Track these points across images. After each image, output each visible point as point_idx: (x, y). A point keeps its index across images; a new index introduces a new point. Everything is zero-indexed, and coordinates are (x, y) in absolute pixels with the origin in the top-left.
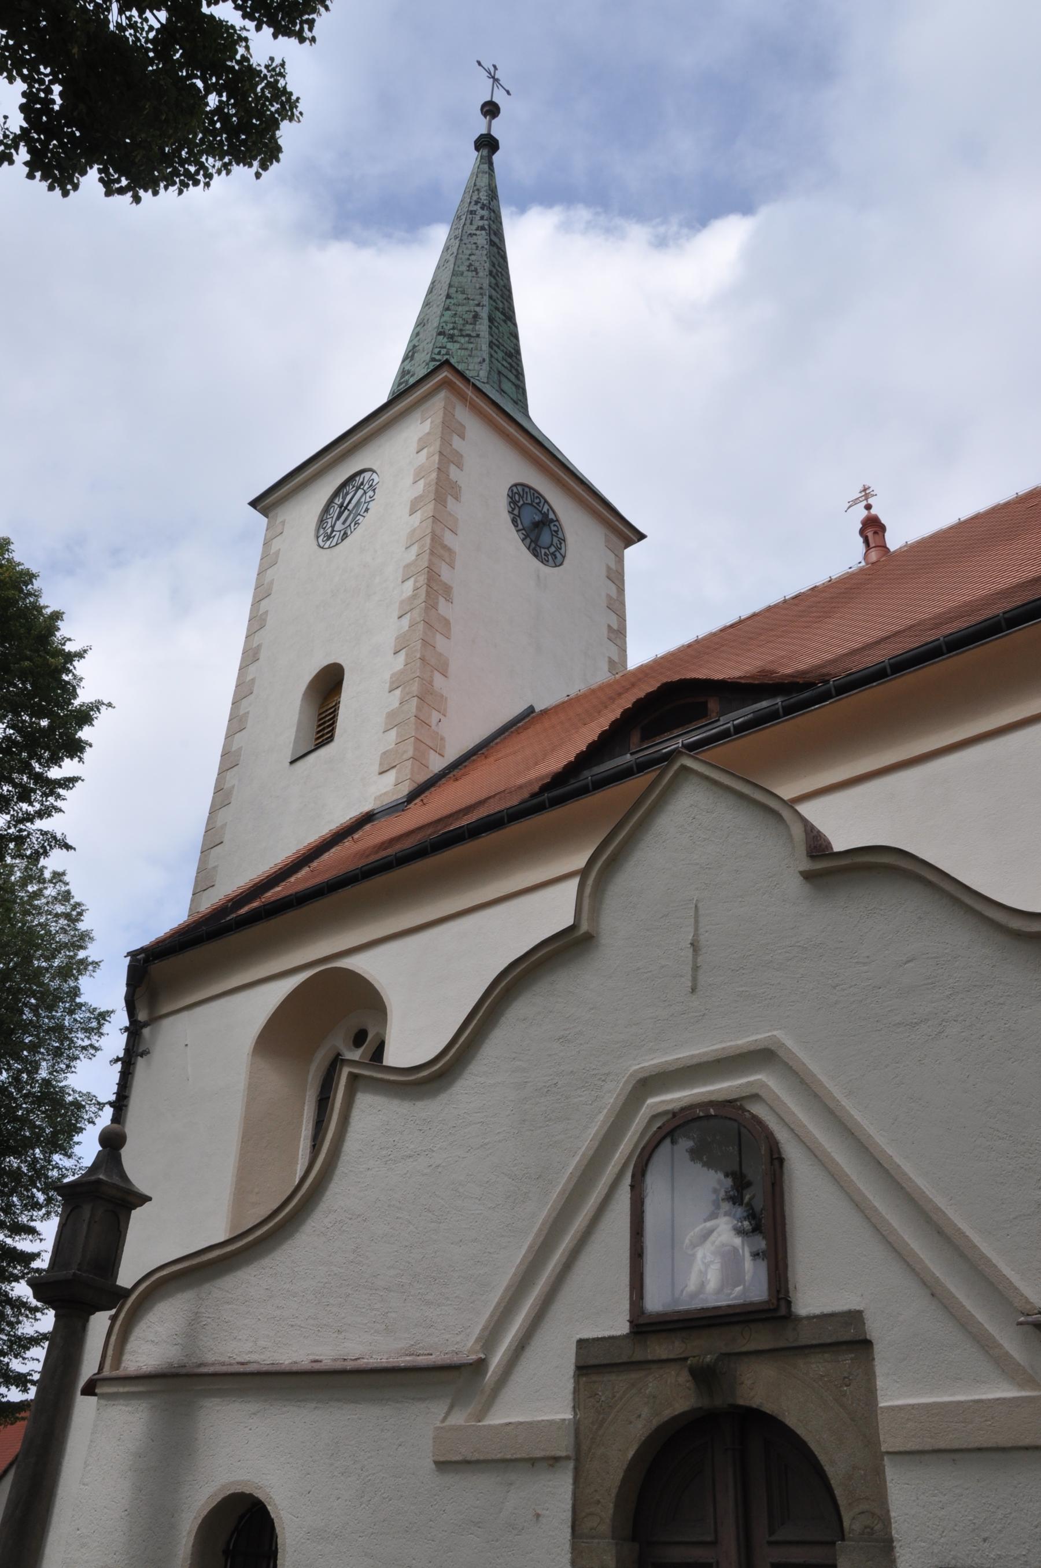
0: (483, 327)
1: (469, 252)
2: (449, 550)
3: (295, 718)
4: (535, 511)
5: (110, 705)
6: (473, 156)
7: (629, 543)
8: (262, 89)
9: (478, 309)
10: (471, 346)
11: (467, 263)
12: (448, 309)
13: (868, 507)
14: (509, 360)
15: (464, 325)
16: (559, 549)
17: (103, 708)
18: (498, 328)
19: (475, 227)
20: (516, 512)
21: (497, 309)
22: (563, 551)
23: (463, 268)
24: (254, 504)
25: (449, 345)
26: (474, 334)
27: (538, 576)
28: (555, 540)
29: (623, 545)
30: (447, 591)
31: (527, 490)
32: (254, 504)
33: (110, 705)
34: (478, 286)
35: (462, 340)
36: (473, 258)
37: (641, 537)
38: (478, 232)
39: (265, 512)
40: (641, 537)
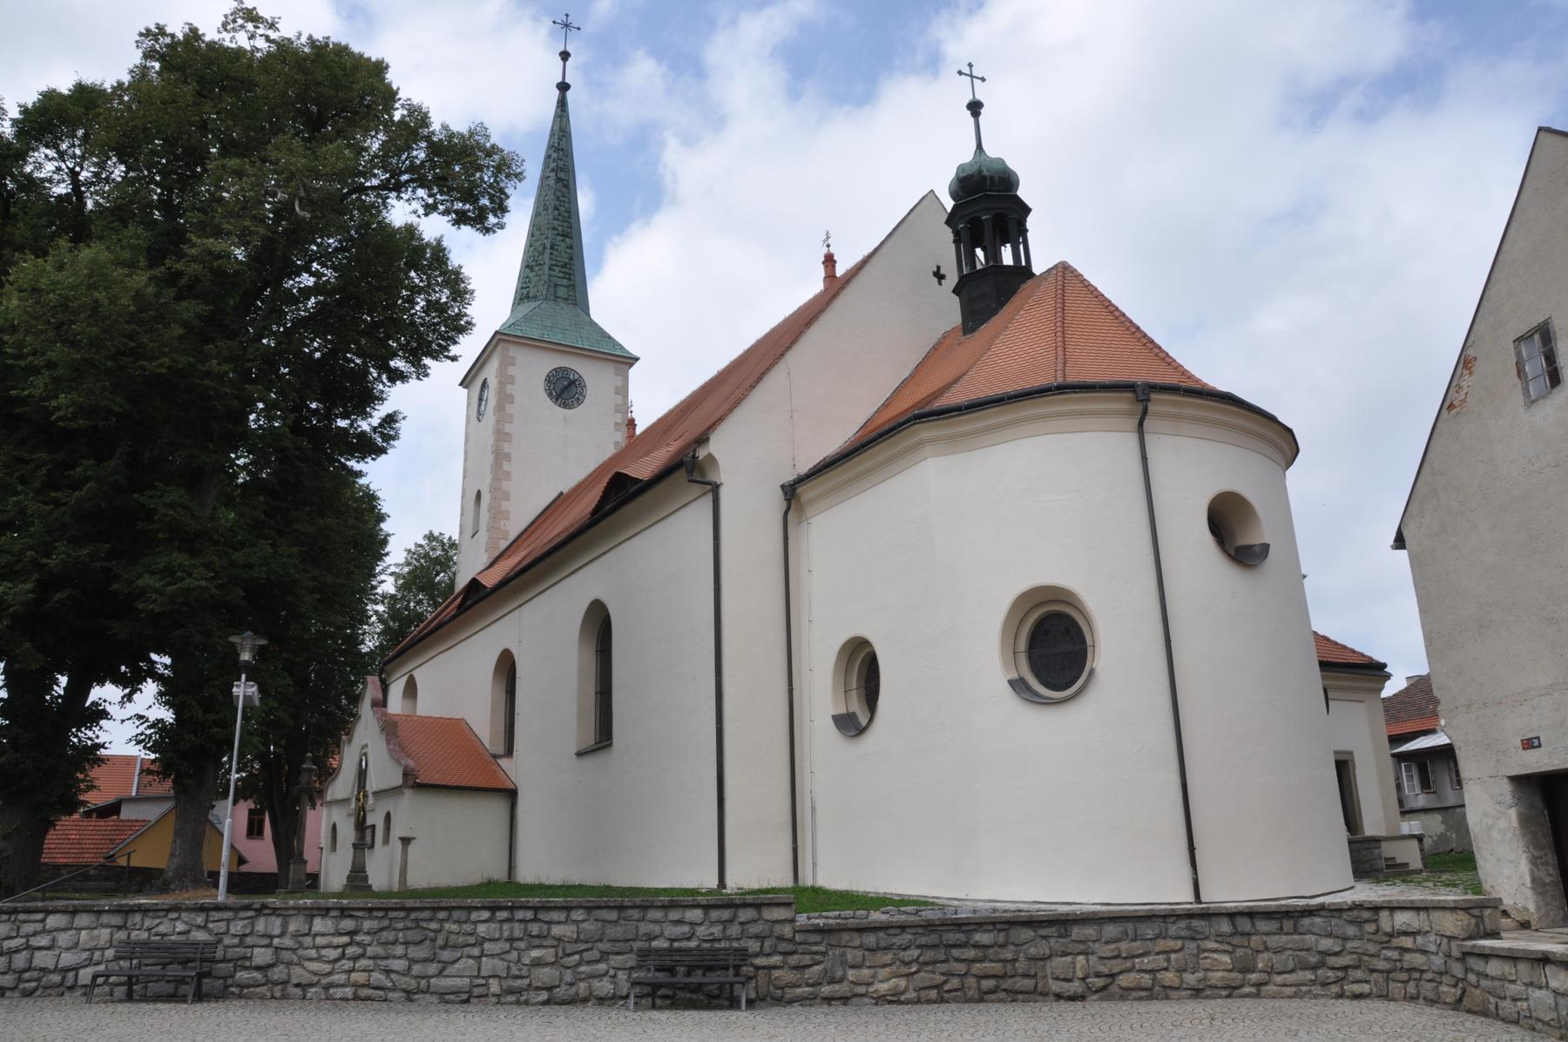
0: (547, 256)
2: (507, 434)
25: (531, 275)
30: (508, 457)
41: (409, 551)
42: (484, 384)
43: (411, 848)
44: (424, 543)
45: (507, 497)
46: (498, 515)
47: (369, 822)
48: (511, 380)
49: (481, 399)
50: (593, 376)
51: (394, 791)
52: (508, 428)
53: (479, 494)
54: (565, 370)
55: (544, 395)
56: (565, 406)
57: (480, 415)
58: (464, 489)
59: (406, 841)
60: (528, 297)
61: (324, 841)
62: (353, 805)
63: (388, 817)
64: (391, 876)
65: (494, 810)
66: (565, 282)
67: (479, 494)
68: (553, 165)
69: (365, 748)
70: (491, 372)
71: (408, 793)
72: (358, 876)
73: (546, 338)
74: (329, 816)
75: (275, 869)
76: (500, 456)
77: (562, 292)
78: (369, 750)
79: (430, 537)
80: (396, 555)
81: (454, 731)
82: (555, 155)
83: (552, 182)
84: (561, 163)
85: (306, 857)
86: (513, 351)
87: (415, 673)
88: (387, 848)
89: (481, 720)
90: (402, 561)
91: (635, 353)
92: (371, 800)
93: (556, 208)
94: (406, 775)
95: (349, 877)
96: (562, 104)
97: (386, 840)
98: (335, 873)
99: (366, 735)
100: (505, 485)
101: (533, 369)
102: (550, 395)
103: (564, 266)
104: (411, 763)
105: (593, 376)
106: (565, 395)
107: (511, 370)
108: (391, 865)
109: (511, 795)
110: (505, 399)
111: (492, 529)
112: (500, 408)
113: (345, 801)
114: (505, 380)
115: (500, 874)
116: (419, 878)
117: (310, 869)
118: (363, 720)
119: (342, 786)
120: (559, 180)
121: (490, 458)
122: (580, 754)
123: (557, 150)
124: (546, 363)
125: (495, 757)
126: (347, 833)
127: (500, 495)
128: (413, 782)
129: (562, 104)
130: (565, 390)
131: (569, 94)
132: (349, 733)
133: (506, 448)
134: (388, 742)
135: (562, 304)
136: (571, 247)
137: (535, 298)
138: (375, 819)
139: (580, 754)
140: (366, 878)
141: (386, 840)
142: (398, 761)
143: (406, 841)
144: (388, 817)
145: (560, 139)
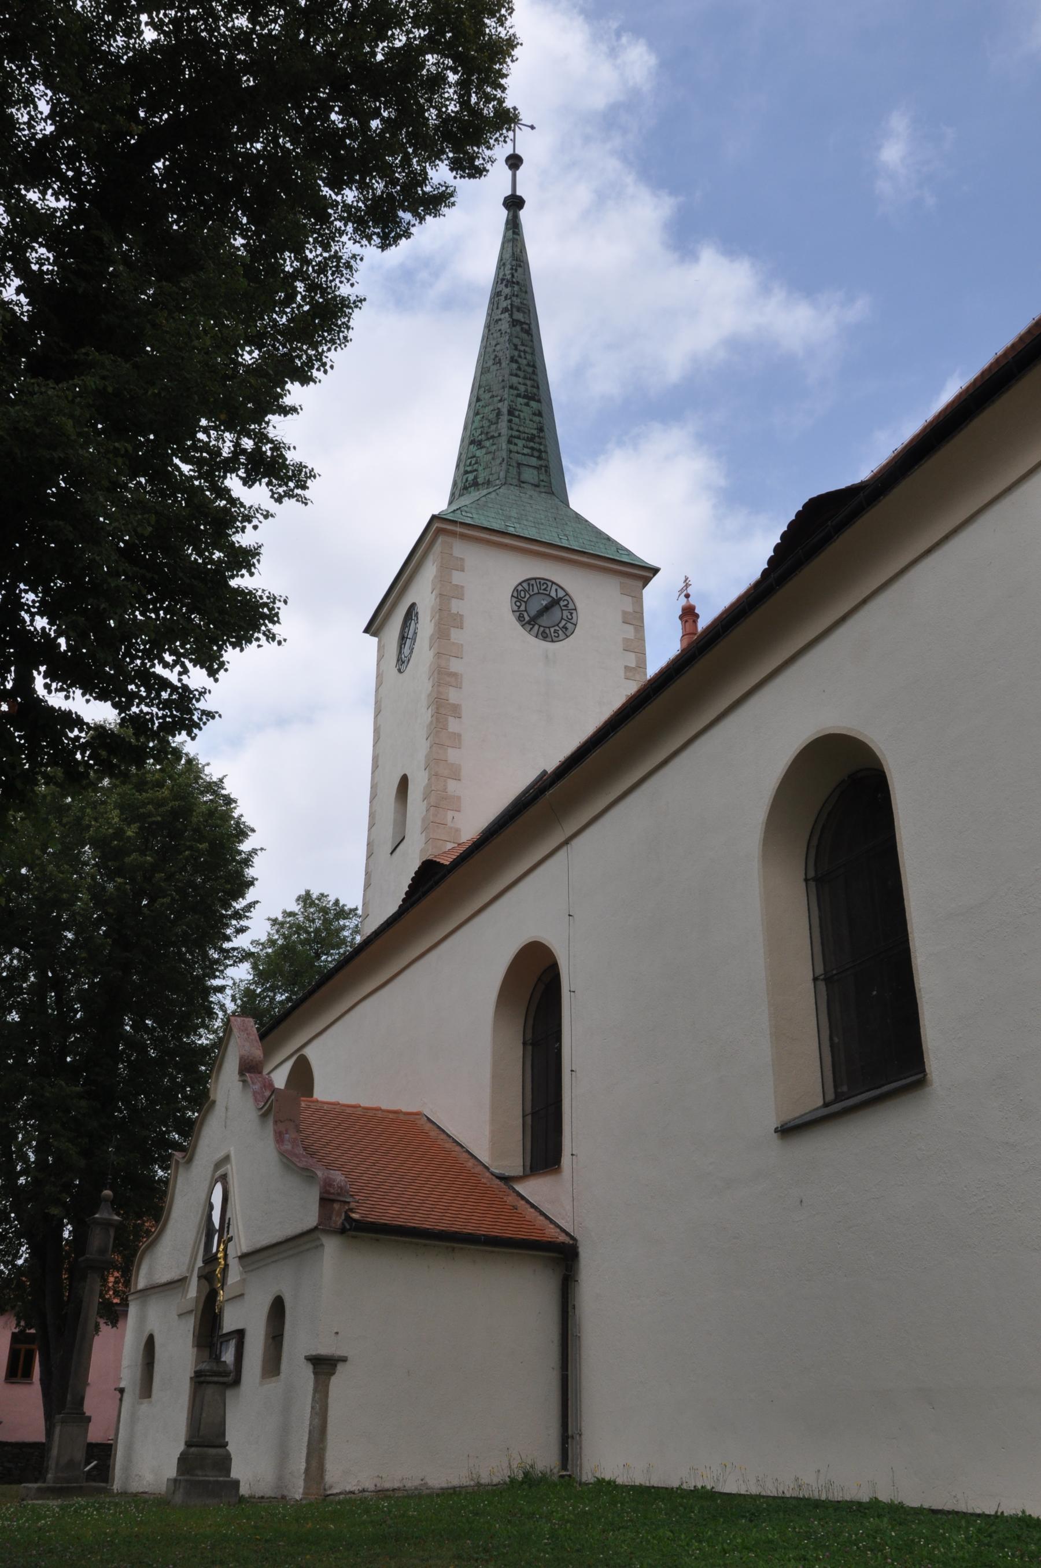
0: (503, 425)
1: (494, 343)
2: (455, 675)
3: (392, 810)
4: (543, 596)
5: (262, 849)
6: (503, 214)
7: (646, 581)
8: (171, 895)
9: (500, 405)
10: (495, 447)
11: (493, 357)
12: (477, 414)
13: (687, 596)
14: (532, 444)
15: (489, 427)
16: (569, 620)
17: (259, 852)
18: (519, 417)
19: (499, 311)
20: (523, 608)
21: (518, 396)
22: (574, 621)
23: (490, 362)
24: (366, 631)
25: (478, 453)
26: (496, 435)
27: (547, 657)
28: (565, 613)
29: (640, 584)
30: (456, 711)
31: (533, 582)
32: (366, 631)
33: (262, 849)
34: (501, 379)
35: (487, 444)
36: (498, 348)
37: (655, 571)
38: (502, 316)
39: (374, 634)
40: (655, 571)
41: (274, 922)
42: (411, 613)
43: (337, 1383)
44: (295, 908)
45: (456, 775)
46: (441, 802)
47: (230, 1323)
48: (459, 593)
49: (403, 638)
50: (590, 596)
51: (295, 1246)
52: (455, 666)
53: (404, 782)
54: (540, 584)
55: (511, 619)
56: (544, 636)
57: (402, 662)
58: (374, 787)
59: (324, 1366)
60: (475, 484)
61: (129, 1375)
62: (192, 1292)
63: (278, 1309)
64: (283, 1456)
65: (509, 1302)
66: (534, 461)
67: (404, 782)
68: (505, 304)
69: (230, 1175)
70: (423, 593)
71: (331, 1248)
72: (205, 1449)
73: (511, 530)
74: (142, 1319)
75: (42, 1438)
76: (442, 711)
77: (529, 475)
78: (233, 1169)
79: (306, 899)
80: (256, 929)
81: (409, 1136)
82: (507, 291)
83: (505, 326)
84: (517, 301)
85: (88, 1408)
86: (461, 549)
87: (309, 1052)
88: (274, 1387)
89: (469, 1105)
90: (264, 938)
91: (651, 560)
92: (234, 1275)
93: (513, 360)
94: (326, 1201)
95: (183, 1459)
96: (514, 226)
97: (273, 1365)
98: (150, 1454)
99: (232, 1130)
100: (455, 606)
101: (491, 580)
102: (520, 618)
103: (532, 438)
104: (338, 1177)
105: (590, 596)
106: (544, 621)
107: (457, 578)
108: (285, 1431)
109: (562, 1257)
110: (448, 622)
111: (429, 825)
112: (442, 634)
113: (180, 1283)
114: (448, 593)
115: (545, 1458)
116: (350, 1471)
117: (95, 1434)
118: (219, 1111)
119: (171, 1255)
120: (514, 323)
121: (426, 716)
122: (787, 1131)
123: (510, 283)
124: (514, 570)
125: (505, 1179)
126: (178, 1355)
127: (441, 769)
128: (351, 1224)
129: (514, 226)
130: (544, 613)
131: (522, 214)
132: (189, 1129)
133: (453, 696)
134: (279, 1138)
135: (530, 491)
136: (540, 414)
137: (488, 483)
138: (244, 1315)
139: (787, 1131)
140: (224, 1463)
141: (273, 1365)
142: (307, 1175)
143: (324, 1366)
144: (278, 1309)
145: (514, 269)
